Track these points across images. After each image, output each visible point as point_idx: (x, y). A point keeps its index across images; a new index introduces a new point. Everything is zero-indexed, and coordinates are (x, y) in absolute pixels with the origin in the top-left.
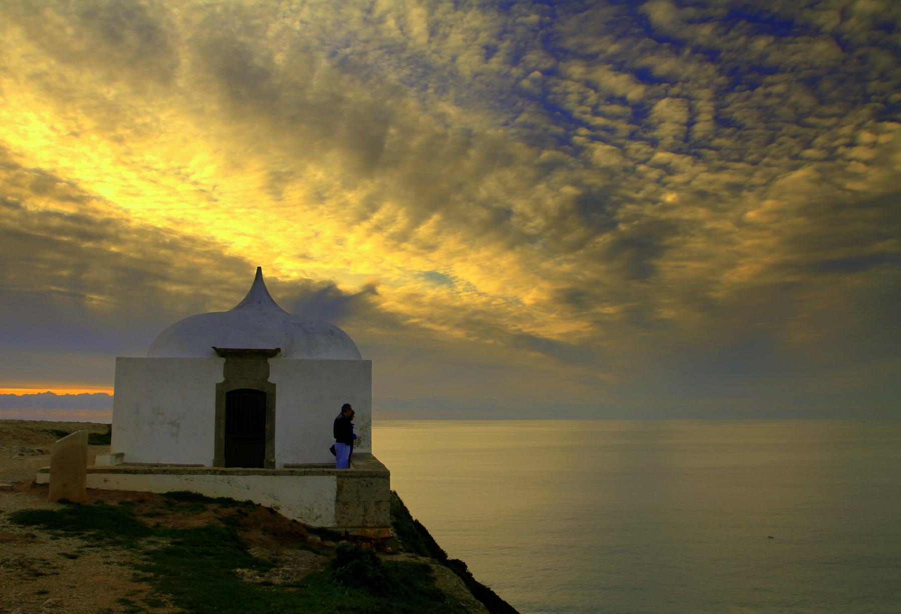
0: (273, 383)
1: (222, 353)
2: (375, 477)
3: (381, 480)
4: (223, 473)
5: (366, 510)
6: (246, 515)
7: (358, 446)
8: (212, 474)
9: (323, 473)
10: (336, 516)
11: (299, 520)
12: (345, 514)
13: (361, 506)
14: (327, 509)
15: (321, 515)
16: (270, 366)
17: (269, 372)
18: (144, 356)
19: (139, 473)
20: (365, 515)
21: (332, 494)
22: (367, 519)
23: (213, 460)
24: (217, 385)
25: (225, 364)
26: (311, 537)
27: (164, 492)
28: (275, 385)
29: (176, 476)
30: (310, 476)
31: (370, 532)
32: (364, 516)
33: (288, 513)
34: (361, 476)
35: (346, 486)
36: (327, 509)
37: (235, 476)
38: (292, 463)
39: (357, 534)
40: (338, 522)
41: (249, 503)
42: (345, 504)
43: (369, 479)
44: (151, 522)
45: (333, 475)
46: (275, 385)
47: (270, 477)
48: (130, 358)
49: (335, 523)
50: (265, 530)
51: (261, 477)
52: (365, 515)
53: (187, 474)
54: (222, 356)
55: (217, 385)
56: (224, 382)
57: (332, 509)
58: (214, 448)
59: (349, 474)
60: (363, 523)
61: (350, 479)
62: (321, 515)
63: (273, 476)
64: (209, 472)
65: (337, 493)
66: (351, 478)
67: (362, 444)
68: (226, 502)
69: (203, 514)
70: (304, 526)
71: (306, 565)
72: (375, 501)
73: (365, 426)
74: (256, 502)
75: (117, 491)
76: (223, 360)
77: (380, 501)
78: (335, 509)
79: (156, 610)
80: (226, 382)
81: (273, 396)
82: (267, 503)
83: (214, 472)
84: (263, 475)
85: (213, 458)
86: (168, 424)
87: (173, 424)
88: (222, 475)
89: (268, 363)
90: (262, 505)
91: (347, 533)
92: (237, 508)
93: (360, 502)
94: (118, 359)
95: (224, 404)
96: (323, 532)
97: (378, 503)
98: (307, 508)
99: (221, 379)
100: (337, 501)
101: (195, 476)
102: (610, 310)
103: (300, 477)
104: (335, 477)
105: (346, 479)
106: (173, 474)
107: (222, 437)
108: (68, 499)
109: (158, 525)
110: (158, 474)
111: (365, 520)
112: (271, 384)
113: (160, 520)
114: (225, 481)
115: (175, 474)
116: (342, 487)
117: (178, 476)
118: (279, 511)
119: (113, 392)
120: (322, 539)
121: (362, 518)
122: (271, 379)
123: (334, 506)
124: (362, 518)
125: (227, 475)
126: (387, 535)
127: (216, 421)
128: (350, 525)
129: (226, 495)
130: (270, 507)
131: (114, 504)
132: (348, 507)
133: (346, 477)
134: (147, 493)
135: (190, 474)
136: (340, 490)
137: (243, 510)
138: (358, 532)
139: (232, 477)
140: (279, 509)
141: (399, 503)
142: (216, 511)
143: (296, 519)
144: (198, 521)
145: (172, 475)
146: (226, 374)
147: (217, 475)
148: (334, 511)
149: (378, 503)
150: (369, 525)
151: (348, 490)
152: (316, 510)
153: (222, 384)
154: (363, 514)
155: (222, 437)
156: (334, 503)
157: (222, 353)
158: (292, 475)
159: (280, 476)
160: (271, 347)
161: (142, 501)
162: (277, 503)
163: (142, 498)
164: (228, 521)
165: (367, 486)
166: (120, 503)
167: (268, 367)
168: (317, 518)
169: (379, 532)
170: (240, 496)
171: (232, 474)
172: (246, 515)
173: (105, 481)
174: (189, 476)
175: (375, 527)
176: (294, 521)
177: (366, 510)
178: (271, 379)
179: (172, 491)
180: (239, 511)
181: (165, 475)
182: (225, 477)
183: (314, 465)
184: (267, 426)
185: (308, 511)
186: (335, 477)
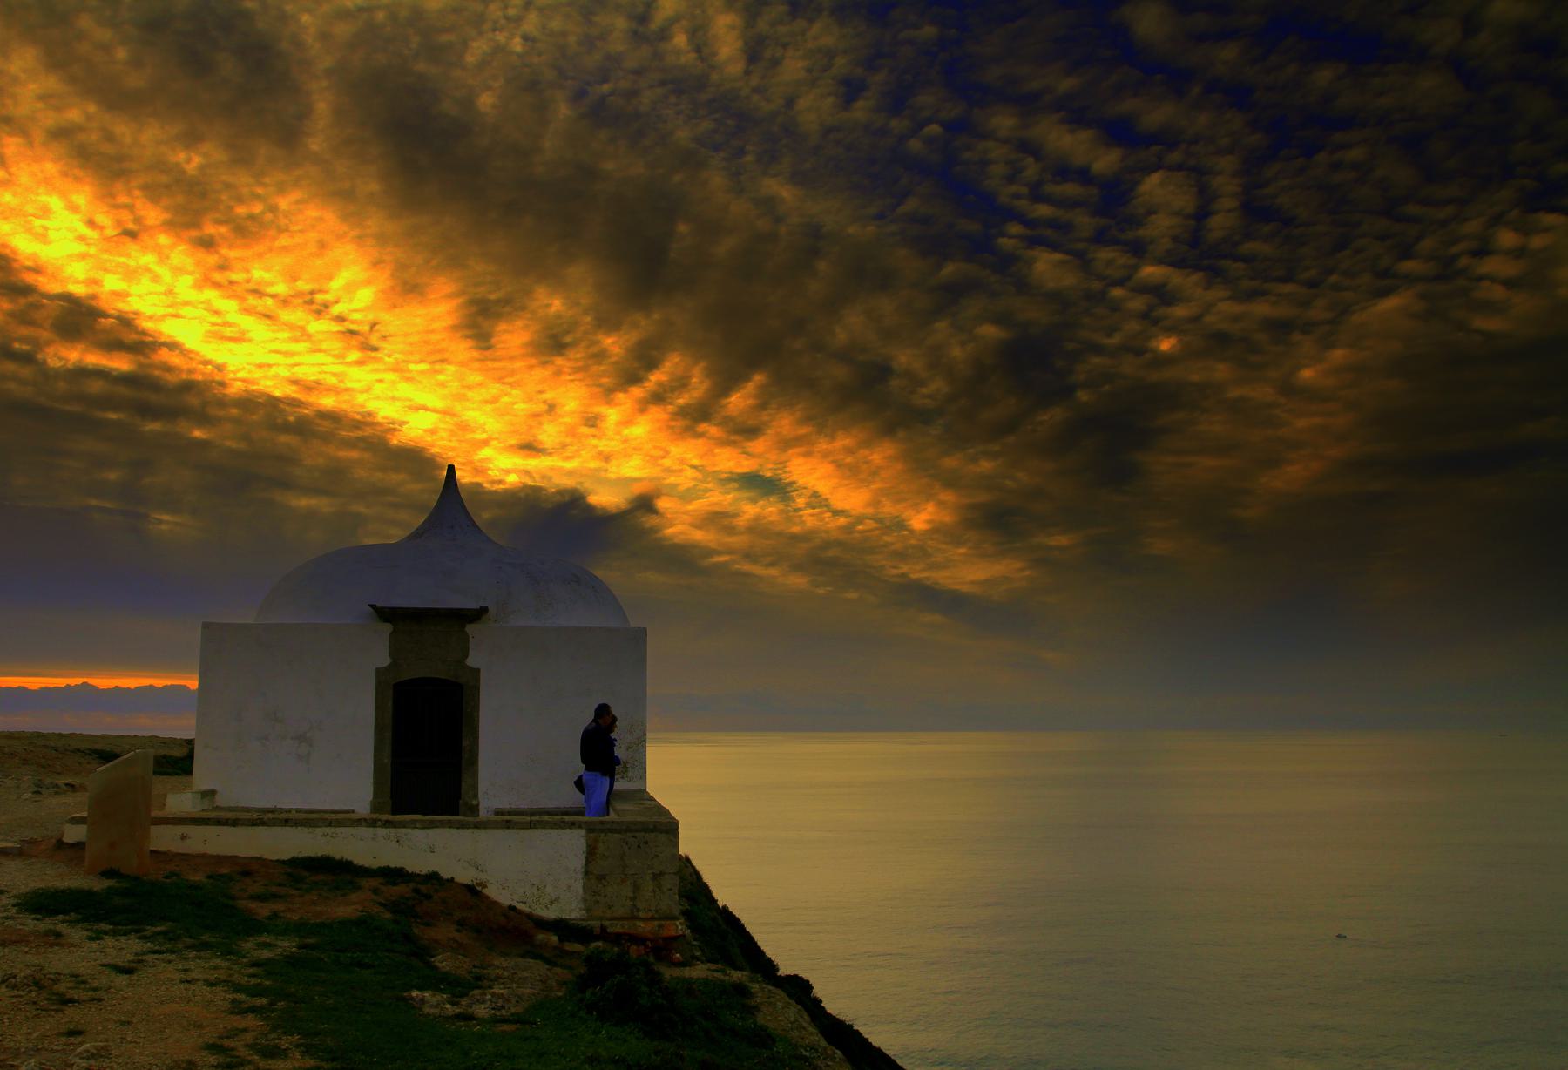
0: (475, 667)
1: (385, 614)
2: (652, 831)
4: (387, 824)
5: (636, 888)
6: (428, 897)
7: (623, 778)
9: (562, 825)
10: (585, 900)
11: (520, 906)
14: (569, 887)
15: (559, 898)
16: (471, 639)
18: (251, 621)
19: (243, 825)
21: (578, 863)
24: (378, 670)
25: (391, 634)
26: (541, 937)
27: (286, 857)
28: (478, 671)
30: (539, 830)
31: (643, 928)
34: (628, 830)
36: (569, 887)
37: (409, 830)
38: (508, 806)
39: (621, 931)
40: (588, 910)
41: (433, 877)
42: (601, 878)
43: (643, 834)
44: (263, 910)
45: (580, 827)
46: (478, 671)
47: (470, 831)
50: (461, 924)
51: (454, 831)
53: (326, 826)
54: (386, 620)
55: (378, 670)
57: (578, 886)
61: (610, 834)
62: (559, 898)
64: (364, 823)
65: (587, 858)
66: (611, 832)
67: (630, 774)
68: (394, 875)
69: (354, 897)
70: (529, 916)
71: (532, 985)
72: (653, 873)
74: (446, 875)
75: (204, 856)
76: (387, 628)
77: (662, 874)
81: (476, 689)
82: (465, 876)
83: (373, 823)
84: (458, 828)
88: (386, 828)
90: (456, 880)
91: (603, 929)
92: (412, 885)
93: (626, 875)
94: (206, 626)
95: (390, 704)
96: (561, 927)
97: (657, 877)
98: (533, 885)
99: (385, 661)
100: (587, 873)
102: (1062, 540)
104: (583, 832)
105: (603, 835)
106: (301, 826)
107: (386, 761)
109: (275, 915)
111: (634, 906)
112: (471, 669)
113: (278, 906)
115: (305, 826)
116: (595, 848)
117: (311, 829)
118: (484, 891)
119: (197, 683)
120: (561, 940)
121: (629, 903)
122: (471, 661)
123: (581, 881)
124: (629, 903)
125: (395, 827)
126: (673, 933)
129: (394, 863)
131: (198, 877)
132: (606, 883)
133: (602, 831)
135: (330, 825)
136: (591, 853)
137: (423, 888)
141: (695, 877)
142: (375, 891)
143: (514, 904)
144: (345, 909)
146: (394, 651)
147: (378, 829)
148: (581, 891)
149: (657, 877)
150: (641, 914)
152: (549, 889)
153: (386, 669)
154: (632, 895)
155: (386, 761)
156: (581, 876)
157: (385, 614)
158: (508, 828)
160: (472, 604)
161: (247, 873)
162: (483, 877)
163: (248, 868)
164: (395, 907)
165: (639, 846)
166: (209, 877)
168: (552, 903)
169: (660, 927)
170: (418, 864)
171: (404, 827)
172: (428, 897)
173: (183, 838)
174: (329, 830)
175: (653, 918)
176: (512, 908)
177: (636, 888)
178: (471, 661)
179: (300, 856)
180: (416, 891)
181: (287, 828)
182: (392, 831)
184: (465, 743)
185: (536, 892)
186: (583, 832)
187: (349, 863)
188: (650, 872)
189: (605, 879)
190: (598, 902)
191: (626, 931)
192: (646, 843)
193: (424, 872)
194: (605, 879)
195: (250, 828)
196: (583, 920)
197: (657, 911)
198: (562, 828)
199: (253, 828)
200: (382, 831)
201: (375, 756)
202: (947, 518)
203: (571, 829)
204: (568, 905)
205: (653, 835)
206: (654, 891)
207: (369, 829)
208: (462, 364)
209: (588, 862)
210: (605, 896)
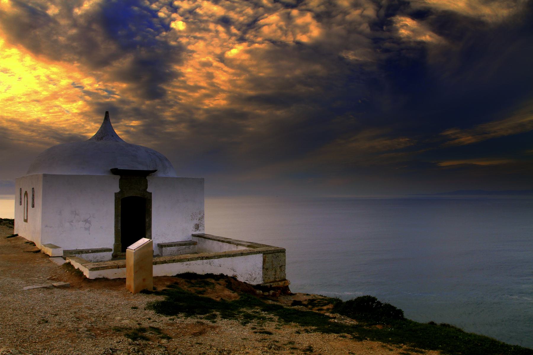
0: (150, 192)
1: (115, 172)
3: (282, 254)
5: (276, 271)
7: (197, 230)
8: (201, 260)
9: (257, 253)
10: (263, 277)
12: (266, 275)
13: (274, 270)
14: (259, 273)
15: (256, 277)
16: (148, 181)
17: (147, 185)
19: (159, 264)
20: (275, 274)
21: (261, 265)
22: (276, 276)
23: (114, 244)
24: (115, 193)
26: (258, 292)
27: (175, 274)
28: (151, 193)
29: (180, 263)
32: (275, 275)
33: (241, 278)
34: (274, 253)
35: (267, 259)
36: (259, 273)
37: (213, 260)
38: (162, 242)
39: (275, 286)
40: (264, 280)
42: (267, 269)
43: (277, 253)
45: (261, 253)
47: (231, 258)
48: (54, 175)
49: (263, 281)
51: (226, 258)
52: (275, 274)
53: (187, 261)
55: (115, 193)
56: (119, 192)
57: (261, 273)
58: (114, 236)
59: (269, 252)
60: (275, 279)
61: (269, 255)
62: (256, 277)
63: (233, 257)
64: (199, 259)
65: (263, 263)
66: (269, 254)
67: (200, 229)
72: (280, 266)
73: (201, 218)
76: (118, 177)
78: (262, 273)
79: (280, 352)
80: (121, 192)
84: (227, 257)
85: (113, 242)
86: (82, 221)
87: (86, 221)
88: (206, 259)
89: (146, 179)
91: (271, 286)
93: (273, 267)
96: (258, 287)
98: (249, 274)
99: (118, 190)
100: (263, 268)
101: (191, 262)
102: (134, 123)
103: (246, 256)
104: (262, 254)
105: (267, 255)
106: (179, 262)
107: (119, 228)
108: (339, 298)
110: (170, 263)
111: (275, 277)
112: (149, 193)
114: (208, 263)
117: (182, 263)
120: (263, 292)
122: (149, 190)
125: (209, 259)
127: (115, 218)
128: (269, 281)
130: (232, 276)
132: (268, 271)
134: (164, 276)
135: (188, 261)
136: (264, 261)
138: (275, 285)
139: (212, 260)
140: (237, 277)
145: (178, 263)
146: (121, 186)
147: (204, 260)
148: (262, 275)
150: (277, 280)
151: (268, 261)
152: (253, 275)
153: (119, 193)
154: (274, 274)
156: (262, 269)
157: (115, 172)
158: (242, 255)
159: (236, 257)
162: (235, 273)
165: (276, 258)
167: (147, 182)
171: (212, 259)
174: (188, 262)
176: (245, 283)
177: (276, 271)
178: (149, 190)
179: (180, 273)
181: (174, 263)
182: (208, 260)
183: (178, 243)
184: (147, 220)
185: (250, 276)
186: (262, 254)
187: (195, 274)
188: (279, 265)
189: (268, 269)
190: (266, 277)
191: (277, 286)
192: (278, 256)
193: (218, 274)
194: (268, 269)
195: (161, 265)
196: (263, 284)
197: (281, 278)
198: (257, 254)
199: (162, 264)
200: (205, 261)
201: (115, 227)
202: (87, 109)
203: (259, 254)
204: (258, 280)
205: (280, 253)
206: (280, 272)
207: (201, 260)
208: (199, 109)
209: (263, 264)
210: (268, 275)
